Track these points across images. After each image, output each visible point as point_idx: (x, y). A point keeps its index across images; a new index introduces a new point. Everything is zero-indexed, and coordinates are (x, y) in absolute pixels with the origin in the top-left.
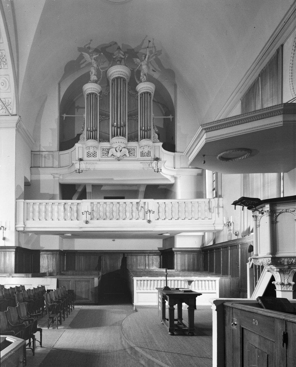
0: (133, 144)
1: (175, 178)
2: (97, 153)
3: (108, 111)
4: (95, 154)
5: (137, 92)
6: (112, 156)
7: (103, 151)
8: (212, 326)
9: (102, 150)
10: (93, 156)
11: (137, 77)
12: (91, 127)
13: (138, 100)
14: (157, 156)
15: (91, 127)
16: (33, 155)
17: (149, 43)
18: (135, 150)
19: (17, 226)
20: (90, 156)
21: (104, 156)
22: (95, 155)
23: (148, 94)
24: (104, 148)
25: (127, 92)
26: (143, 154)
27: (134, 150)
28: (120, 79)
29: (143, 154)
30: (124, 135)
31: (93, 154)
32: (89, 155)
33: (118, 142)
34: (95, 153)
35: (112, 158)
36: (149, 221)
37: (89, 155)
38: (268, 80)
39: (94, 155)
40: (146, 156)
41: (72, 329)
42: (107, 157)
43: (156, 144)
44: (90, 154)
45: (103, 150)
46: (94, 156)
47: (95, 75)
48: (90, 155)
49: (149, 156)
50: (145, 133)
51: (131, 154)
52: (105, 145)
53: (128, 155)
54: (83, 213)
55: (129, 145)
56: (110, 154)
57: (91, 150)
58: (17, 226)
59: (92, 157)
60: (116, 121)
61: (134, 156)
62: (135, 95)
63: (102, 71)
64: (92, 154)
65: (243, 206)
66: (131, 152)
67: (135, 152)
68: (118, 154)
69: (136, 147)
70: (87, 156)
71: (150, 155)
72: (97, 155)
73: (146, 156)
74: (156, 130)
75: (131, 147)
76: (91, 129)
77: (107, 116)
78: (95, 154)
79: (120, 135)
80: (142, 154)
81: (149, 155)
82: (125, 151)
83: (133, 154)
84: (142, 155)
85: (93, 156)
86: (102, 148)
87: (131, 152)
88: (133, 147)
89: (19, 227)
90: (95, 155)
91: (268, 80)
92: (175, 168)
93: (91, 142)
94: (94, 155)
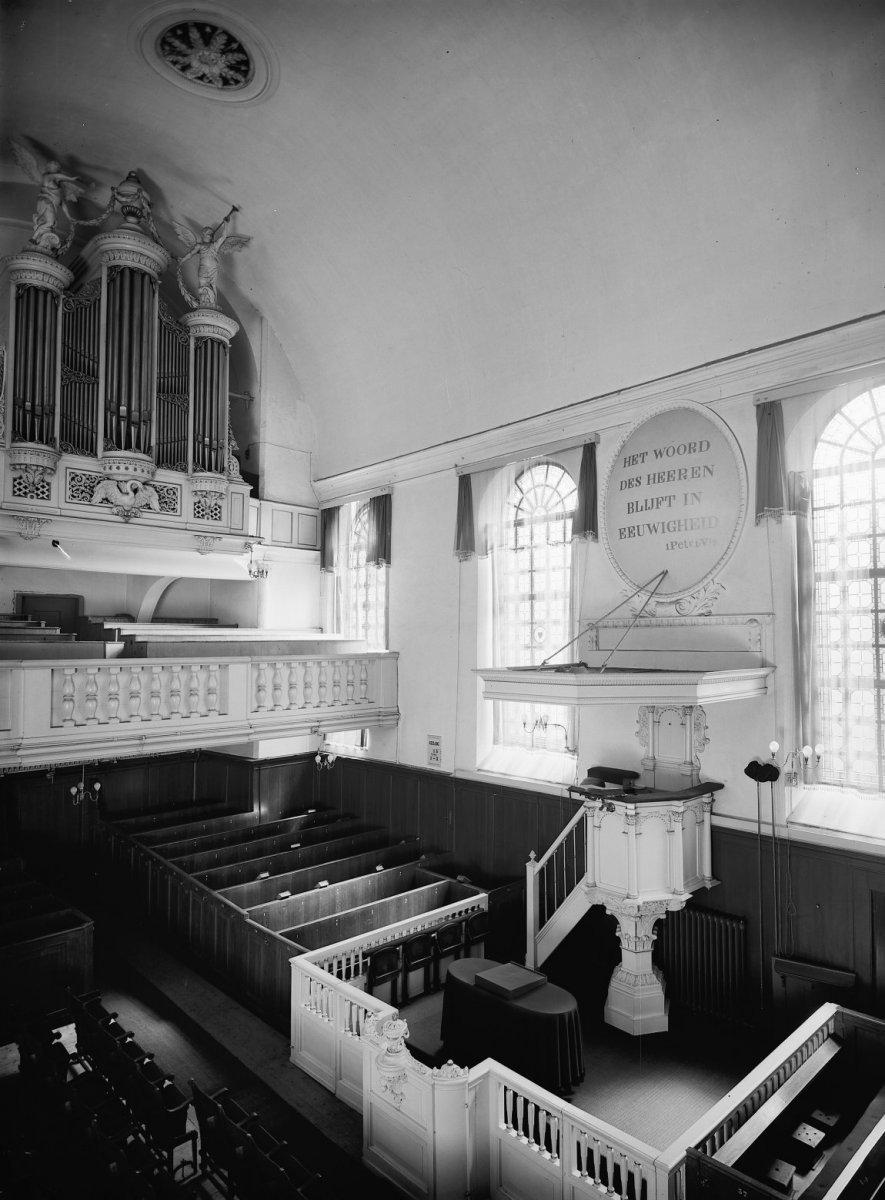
0: (167, 477)
3: (78, 350)
5: (186, 329)
7: (73, 483)
9: (69, 479)
10: (38, 495)
18: (178, 494)
21: (75, 501)
22: (216, 514)
23: (221, 347)
24: (78, 472)
25: (156, 321)
26: (21, 487)
27: (174, 493)
30: (148, 451)
31: (38, 489)
33: (128, 465)
35: (104, 512)
38: (468, 1175)
41: (490, 485)
43: (234, 488)
44: (24, 484)
45: (73, 479)
46: (41, 495)
47: (52, 230)
49: (44, 496)
50: (210, 454)
53: (155, 505)
56: (98, 497)
59: (32, 497)
60: (124, 400)
64: (208, 511)
66: (167, 500)
68: (127, 500)
70: (14, 492)
71: (16, 483)
74: (233, 447)
75: (165, 485)
79: (138, 446)
80: (199, 511)
81: (43, 493)
84: (20, 490)
85: (38, 495)
86: (69, 471)
90: (216, 514)
91: (468, 1175)
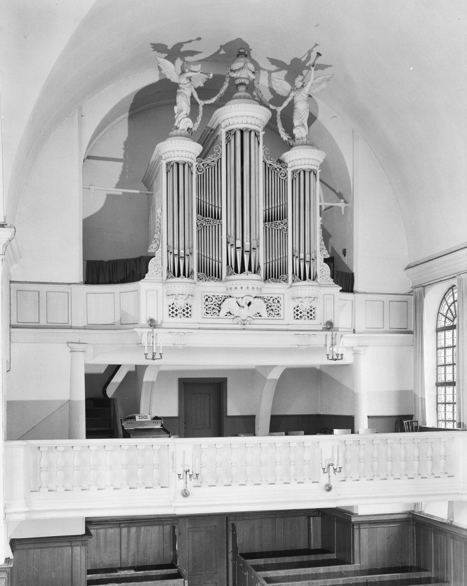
1: (356, 353)
2: (193, 307)
4: (188, 311)
6: (229, 314)
8: (223, 436)
10: (184, 315)
11: (284, 126)
12: (181, 246)
13: (286, 182)
14: (446, 472)
15: (181, 246)
16: (13, 293)
17: (316, 58)
19: (8, 510)
20: (176, 315)
24: (210, 295)
27: (278, 302)
28: (248, 133)
29: (298, 313)
32: (173, 313)
34: (188, 306)
36: (329, 489)
37: (173, 312)
39: (187, 312)
40: (305, 319)
42: (216, 316)
45: (207, 300)
46: (186, 315)
48: (175, 313)
51: (271, 312)
52: (212, 287)
53: (264, 313)
54: (179, 475)
55: (264, 290)
57: (180, 304)
58: (8, 510)
61: (277, 317)
62: (280, 169)
63: (203, 104)
65: (250, 81)
67: (282, 307)
69: (283, 294)
72: (193, 313)
73: (305, 319)
76: (182, 251)
77: (215, 218)
78: (187, 308)
82: (259, 306)
83: (277, 313)
86: (204, 294)
87: (273, 308)
88: (275, 296)
89: (10, 513)
92: (354, 333)
93: (181, 285)
94: (187, 312)
